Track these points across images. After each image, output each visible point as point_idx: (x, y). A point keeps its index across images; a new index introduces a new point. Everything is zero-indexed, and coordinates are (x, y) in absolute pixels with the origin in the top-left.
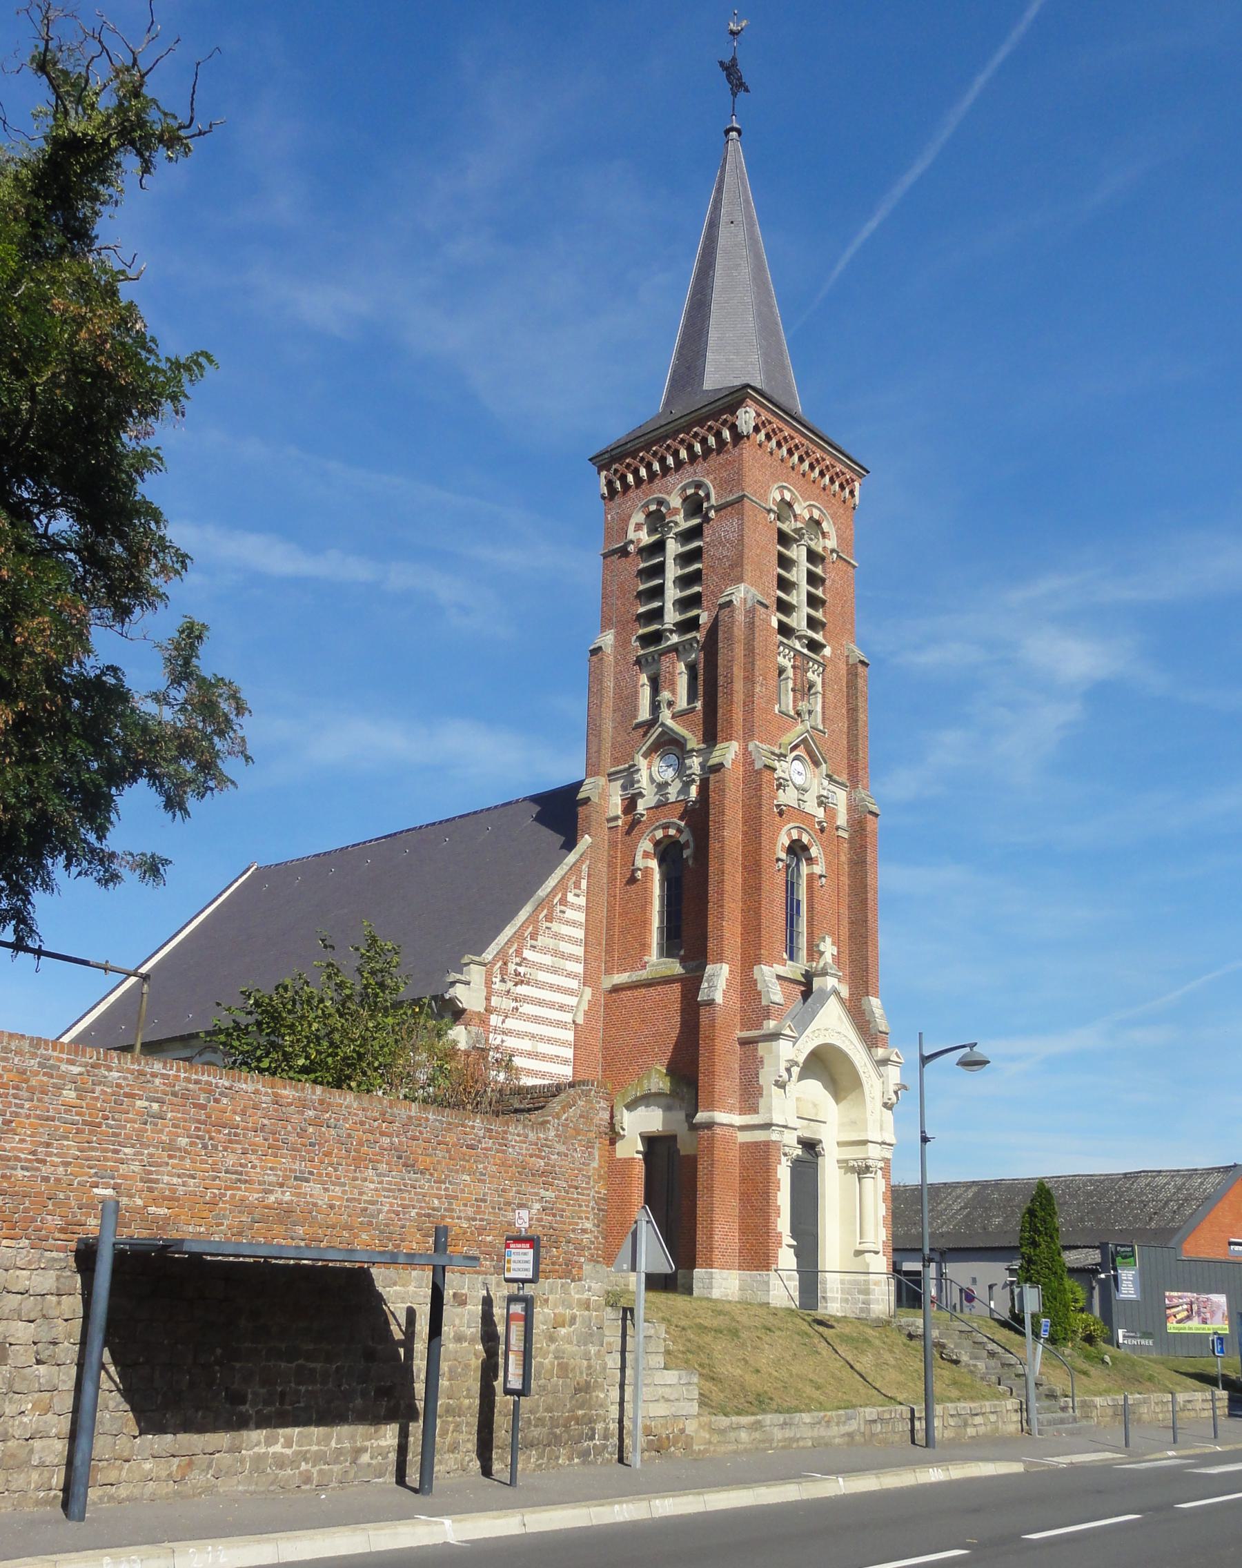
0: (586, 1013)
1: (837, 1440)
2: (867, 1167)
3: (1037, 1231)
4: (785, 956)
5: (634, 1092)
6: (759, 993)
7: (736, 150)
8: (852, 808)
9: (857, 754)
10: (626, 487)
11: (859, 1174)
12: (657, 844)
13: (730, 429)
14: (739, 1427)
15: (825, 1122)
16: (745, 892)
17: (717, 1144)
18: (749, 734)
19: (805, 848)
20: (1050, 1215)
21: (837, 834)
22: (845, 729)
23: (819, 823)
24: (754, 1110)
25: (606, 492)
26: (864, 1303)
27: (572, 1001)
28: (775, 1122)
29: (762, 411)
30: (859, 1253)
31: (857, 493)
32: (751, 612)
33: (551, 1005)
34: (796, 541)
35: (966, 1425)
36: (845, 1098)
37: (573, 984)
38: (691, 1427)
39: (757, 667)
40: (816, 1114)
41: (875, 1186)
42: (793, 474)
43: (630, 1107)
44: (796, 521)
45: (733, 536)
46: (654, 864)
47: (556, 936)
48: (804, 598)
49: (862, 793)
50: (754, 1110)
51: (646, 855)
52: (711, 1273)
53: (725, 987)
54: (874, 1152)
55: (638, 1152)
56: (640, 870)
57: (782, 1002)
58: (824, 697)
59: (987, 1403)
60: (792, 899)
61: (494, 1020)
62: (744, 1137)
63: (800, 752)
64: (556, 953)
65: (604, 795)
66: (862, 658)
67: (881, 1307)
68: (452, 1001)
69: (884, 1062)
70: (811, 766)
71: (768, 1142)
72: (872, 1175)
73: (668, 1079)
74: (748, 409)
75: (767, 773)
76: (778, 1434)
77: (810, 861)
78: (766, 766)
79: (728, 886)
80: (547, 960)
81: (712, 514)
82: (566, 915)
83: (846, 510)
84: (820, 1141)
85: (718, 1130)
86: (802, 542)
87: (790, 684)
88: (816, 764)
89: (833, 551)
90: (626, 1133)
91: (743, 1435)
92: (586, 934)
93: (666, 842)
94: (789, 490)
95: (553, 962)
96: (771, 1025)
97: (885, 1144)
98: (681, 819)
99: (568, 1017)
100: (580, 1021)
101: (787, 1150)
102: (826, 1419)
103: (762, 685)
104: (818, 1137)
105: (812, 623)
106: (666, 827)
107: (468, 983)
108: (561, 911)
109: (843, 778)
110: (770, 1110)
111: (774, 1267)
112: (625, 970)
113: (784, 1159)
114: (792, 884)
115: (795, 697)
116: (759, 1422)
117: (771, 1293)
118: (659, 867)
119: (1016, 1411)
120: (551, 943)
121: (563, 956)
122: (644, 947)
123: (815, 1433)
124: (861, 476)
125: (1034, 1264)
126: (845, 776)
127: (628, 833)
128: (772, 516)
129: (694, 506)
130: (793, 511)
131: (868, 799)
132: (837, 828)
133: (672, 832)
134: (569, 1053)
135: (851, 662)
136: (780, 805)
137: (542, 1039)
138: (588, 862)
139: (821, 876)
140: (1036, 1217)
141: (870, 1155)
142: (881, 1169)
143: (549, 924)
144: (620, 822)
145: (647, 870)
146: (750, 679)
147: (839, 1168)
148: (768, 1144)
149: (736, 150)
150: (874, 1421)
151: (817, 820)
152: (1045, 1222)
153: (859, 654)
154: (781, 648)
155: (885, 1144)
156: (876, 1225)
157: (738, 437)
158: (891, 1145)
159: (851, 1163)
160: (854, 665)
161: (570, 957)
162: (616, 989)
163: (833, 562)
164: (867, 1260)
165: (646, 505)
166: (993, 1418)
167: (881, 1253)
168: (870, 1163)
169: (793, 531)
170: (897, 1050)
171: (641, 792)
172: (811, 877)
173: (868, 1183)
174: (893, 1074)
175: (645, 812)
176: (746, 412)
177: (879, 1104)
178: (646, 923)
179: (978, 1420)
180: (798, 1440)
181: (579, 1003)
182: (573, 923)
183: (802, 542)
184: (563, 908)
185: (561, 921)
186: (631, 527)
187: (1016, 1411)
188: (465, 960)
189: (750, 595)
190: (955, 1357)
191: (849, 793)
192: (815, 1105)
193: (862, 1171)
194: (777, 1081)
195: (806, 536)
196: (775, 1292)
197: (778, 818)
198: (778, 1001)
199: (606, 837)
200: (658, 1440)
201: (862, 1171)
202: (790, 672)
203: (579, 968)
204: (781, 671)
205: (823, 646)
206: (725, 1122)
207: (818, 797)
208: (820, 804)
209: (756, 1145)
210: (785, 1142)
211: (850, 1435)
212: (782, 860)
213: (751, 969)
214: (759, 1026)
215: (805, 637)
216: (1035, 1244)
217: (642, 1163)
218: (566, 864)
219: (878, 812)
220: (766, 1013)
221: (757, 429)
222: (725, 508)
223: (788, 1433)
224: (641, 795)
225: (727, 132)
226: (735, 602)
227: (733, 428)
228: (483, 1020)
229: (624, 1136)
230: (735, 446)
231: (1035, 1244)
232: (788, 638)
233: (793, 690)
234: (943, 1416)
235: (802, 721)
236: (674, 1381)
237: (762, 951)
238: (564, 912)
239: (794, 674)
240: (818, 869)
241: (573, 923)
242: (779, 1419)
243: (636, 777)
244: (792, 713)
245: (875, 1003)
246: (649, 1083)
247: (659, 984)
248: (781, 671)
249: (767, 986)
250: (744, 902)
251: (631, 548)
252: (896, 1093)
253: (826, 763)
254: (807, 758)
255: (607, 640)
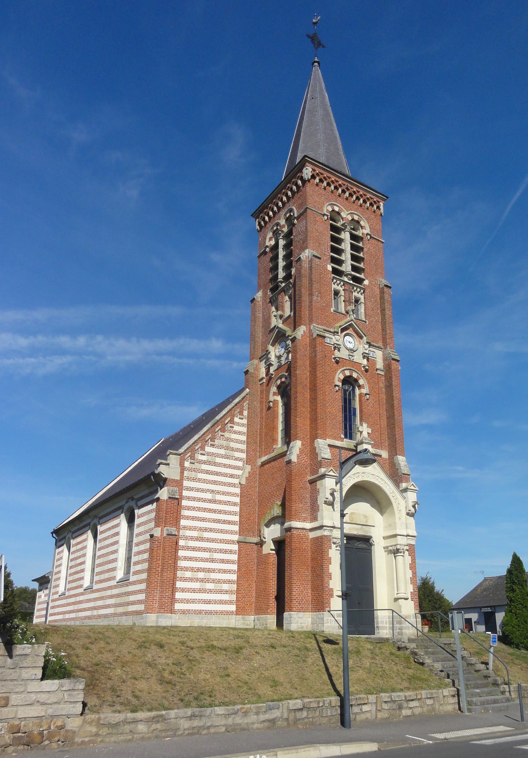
0: (247, 479)
1: (255, 726)
2: (398, 550)
3: (513, 583)
4: (343, 436)
5: (268, 517)
6: (317, 454)
7: (317, 72)
8: (385, 359)
9: (386, 331)
10: (266, 223)
11: (394, 554)
12: (279, 387)
13: (300, 180)
14: (135, 721)
15: (374, 526)
16: (311, 402)
17: (295, 540)
18: (311, 321)
19: (356, 381)
20: (520, 573)
21: (377, 373)
22: (380, 320)
23: (364, 367)
24: (314, 519)
25: (259, 228)
26: (399, 629)
27: (239, 472)
28: (325, 524)
29: (316, 168)
30: (396, 600)
31: (382, 207)
32: (311, 261)
33: (225, 475)
34: (343, 230)
35: (400, 708)
36: (385, 512)
37: (240, 464)
38: (73, 724)
39: (314, 288)
40: (367, 522)
41: (404, 560)
42: (340, 199)
43: (268, 525)
44: (343, 221)
45: (303, 229)
46: (279, 398)
47: (228, 439)
48: (349, 256)
49: (389, 350)
50: (314, 519)
51: (274, 394)
52: (291, 614)
53: (298, 453)
54: (402, 541)
55: (271, 550)
56: (272, 402)
57: (330, 457)
58: (365, 304)
59: (423, 692)
60: (350, 408)
61: (186, 483)
62: (312, 535)
63: (350, 331)
64: (227, 448)
65: (257, 369)
66: (386, 284)
67: (411, 631)
68: (159, 474)
69: (406, 490)
70: (358, 339)
71: (322, 536)
72: (402, 554)
73: (281, 507)
74: (307, 167)
75: (319, 339)
76: (185, 724)
77: (360, 387)
78: (318, 335)
79: (300, 399)
80: (222, 452)
81: (296, 221)
82: (234, 429)
83: (376, 216)
84: (371, 537)
85: (294, 532)
86: (347, 230)
87: (342, 298)
88: (361, 337)
89: (367, 234)
90: (266, 540)
91: (141, 727)
92: (247, 438)
93: (283, 385)
94: (337, 206)
95: (226, 452)
96: (322, 470)
97: (409, 536)
98: (286, 372)
99: (236, 481)
100: (244, 482)
101: (335, 540)
102: (243, 710)
103: (317, 296)
104: (369, 534)
105: (354, 268)
106: (281, 378)
107: (168, 464)
108: (230, 427)
109: (380, 344)
110: (322, 518)
111: (327, 609)
112: (267, 454)
113: (333, 546)
114: (350, 400)
115: (345, 304)
116: (162, 716)
117: (325, 625)
118: (282, 399)
119: (453, 696)
120: (225, 443)
121: (232, 449)
122: (275, 441)
123: (230, 721)
124: (384, 200)
125: (513, 602)
126: (381, 344)
127: (268, 385)
128: (326, 217)
129: (289, 220)
130: (341, 216)
131: (392, 353)
132: (377, 370)
133: (283, 379)
134: (237, 500)
135: (381, 287)
136: (336, 358)
137: (219, 493)
138: (247, 402)
139: (366, 394)
140: (513, 574)
141: (399, 542)
142: (407, 550)
143: (222, 434)
144: (264, 381)
145: (275, 402)
146: (311, 295)
147: (385, 551)
148: (322, 537)
149: (317, 72)
150: (301, 710)
151: (362, 365)
152: (517, 577)
153: (384, 282)
154: (335, 281)
155: (409, 536)
156: (406, 583)
157: (304, 182)
158: (414, 537)
159: (390, 548)
160: (383, 288)
161: (238, 450)
162: (263, 464)
163: (368, 240)
164: (400, 604)
165: (272, 228)
166: (429, 702)
167: (410, 599)
168: (398, 547)
169: (341, 225)
170: (413, 483)
171: (270, 363)
172: (360, 395)
173: (400, 558)
174: (412, 497)
175: (273, 373)
176: (306, 169)
177: (404, 513)
178: (275, 428)
179: (412, 704)
180: (208, 728)
181: (243, 473)
182: (239, 433)
183: (347, 230)
184: (232, 425)
185: (230, 432)
186: (267, 240)
187: (453, 696)
188: (168, 453)
189: (310, 254)
190: (421, 661)
191: (383, 352)
192: (366, 517)
193: (396, 552)
194: (325, 501)
195: (348, 227)
196: (329, 624)
197: (335, 365)
198: (326, 457)
199: (259, 389)
200: (27, 736)
201: (396, 552)
202: (342, 293)
203: (244, 456)
204: (336, 293)
205: (364, 280)
206: (299, 527)
207: (362, 354)
208: (364, 357)
209: (317, 538)
210: (334, 536)
211: (273, 721)
212: (338, 386)
213: (313, 442)
214: (317, 472)
215: (351, 275)
216: (513, 590)
217: (275, 556)
218: (233, 403)
219: (398, 359)
220: (320, 465)
221: (313, 177)
222: (300, 217)
223: (196, 723)
224: (272, 365)
225: (313, 64)
226: (302, 258)
227: (302, 178)
228: (179, 484)
229: (265, 542)
230: (303, 187)
231: (513, 590)
232: (341, 277)
233: (344, 301)
234: (376, 703)
235: (349, 316)
236: (54, 688)
237: (318, 432)
238: (233, 427)
239: (345, 293)
240: (364, 391)
241: (239, 433)
242: (186, 713)
243: (269, 356)
244: (344, 312)
245: (401, 460)
246: (274, 511)
247: (279, 458)
248: (336, 293)
249: (321, 450)
250: (311, 408)
251: (268, 250)
252: (414, 507)
253: (366, 336)
254: (355, 335)
255: (259, 295)
